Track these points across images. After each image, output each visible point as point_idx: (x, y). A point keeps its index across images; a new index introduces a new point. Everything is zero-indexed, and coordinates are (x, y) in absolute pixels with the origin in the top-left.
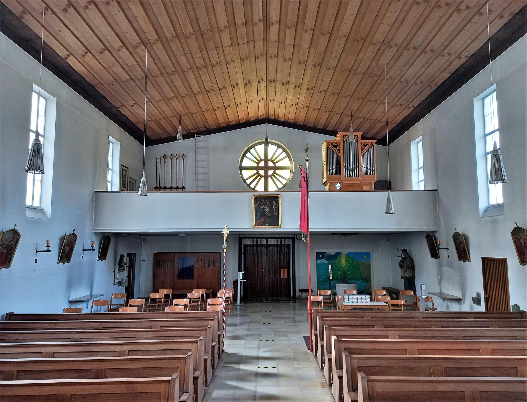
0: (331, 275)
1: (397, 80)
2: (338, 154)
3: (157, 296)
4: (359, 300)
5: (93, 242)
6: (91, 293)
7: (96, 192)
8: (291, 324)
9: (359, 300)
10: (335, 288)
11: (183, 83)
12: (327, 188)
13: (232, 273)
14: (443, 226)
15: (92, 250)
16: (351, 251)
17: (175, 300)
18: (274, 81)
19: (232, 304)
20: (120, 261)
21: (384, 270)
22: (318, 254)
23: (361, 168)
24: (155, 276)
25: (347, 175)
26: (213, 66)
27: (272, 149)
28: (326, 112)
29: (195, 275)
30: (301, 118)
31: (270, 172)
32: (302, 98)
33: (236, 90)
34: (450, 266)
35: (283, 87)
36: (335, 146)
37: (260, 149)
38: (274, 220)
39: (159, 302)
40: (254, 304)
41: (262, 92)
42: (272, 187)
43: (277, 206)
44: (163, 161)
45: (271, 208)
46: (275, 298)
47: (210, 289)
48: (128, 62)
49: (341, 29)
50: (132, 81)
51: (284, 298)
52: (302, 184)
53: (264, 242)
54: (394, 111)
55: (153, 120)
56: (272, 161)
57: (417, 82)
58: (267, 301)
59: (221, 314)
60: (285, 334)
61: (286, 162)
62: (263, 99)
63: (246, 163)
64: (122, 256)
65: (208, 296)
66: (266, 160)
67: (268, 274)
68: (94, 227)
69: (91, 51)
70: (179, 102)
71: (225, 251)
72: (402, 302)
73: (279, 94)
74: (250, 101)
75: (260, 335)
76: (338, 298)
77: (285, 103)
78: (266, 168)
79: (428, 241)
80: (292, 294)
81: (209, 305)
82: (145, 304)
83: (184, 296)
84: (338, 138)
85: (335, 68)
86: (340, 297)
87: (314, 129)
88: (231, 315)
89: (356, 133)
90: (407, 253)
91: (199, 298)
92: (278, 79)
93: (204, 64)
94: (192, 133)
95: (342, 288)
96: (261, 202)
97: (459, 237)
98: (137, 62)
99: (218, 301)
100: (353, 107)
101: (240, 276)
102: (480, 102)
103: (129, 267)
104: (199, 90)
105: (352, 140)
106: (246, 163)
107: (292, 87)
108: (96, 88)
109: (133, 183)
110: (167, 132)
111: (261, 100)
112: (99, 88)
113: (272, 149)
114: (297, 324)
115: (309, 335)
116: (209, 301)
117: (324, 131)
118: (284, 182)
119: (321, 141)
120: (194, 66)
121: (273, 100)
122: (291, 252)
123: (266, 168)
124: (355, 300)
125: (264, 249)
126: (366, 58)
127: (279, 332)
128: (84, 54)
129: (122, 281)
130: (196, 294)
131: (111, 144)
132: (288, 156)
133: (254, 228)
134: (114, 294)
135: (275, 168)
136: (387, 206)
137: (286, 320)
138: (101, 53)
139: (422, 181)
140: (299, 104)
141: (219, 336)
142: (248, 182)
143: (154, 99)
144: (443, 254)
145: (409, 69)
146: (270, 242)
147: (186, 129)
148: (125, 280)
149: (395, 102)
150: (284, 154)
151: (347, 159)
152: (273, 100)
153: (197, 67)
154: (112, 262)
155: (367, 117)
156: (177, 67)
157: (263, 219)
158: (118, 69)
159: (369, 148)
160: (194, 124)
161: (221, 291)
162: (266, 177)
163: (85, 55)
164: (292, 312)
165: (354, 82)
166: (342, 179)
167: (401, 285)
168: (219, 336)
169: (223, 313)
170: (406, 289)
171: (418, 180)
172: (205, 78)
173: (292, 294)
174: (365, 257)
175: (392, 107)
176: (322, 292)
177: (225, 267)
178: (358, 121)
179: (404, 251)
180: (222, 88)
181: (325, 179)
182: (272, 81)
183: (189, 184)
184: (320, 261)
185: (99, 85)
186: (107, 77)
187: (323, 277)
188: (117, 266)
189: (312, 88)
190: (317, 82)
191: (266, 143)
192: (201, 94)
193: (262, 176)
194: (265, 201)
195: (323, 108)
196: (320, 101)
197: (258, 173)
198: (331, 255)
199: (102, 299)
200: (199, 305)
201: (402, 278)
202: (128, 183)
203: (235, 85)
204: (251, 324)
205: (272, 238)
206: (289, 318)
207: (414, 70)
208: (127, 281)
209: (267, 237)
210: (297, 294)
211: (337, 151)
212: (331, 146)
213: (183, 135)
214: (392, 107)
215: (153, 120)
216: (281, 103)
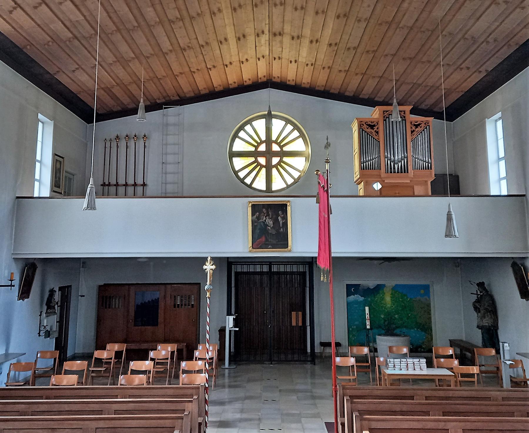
1: (460, 36)
2: (376, 137)
3: (104, 355)
4: (411, 366)
5: (12, 274)
6: (7, 350)
7: (18, 198)
8: (306, 402)
9: (411, 366)
10: (375, 341)
11: (148, 40)
12: (361, 189)
13: (217, 317)
15: (11, 286)
16: (399, 283)
17: (132, 363)
18: (280, 34)
19: (216, 368)
20: (48, 299)
21: (451, 316)
23: (410, 159)
24: (99, 320)
25: (391, 171)
26: (192, 18)
27: (277, 125)
28: (357, 74)
29: (161, 319)
30: (321, 80)
31: (275, 160)
32: (321, 56)
33: (224, 47)
35: (294, 42)
36: (372, 127)
37: (260, 125)
38: (282, 240)
39: (107, 363)
40: (252, 366)
41: (263, 48)
42: (278, 184)
43: (285, 218)
44: (114, 144)
45: (276, 221)
46: (283, 357)
47: (183, 342)
48: (71, 17)
50: (76, 41)
51: (296, 357)
52: (320, 188)
53: (265, 269)
54: (457, 77)
55: (102, 89)
56: (278, 147)
57: (489, 39)
58: (271, 361)
59: (202, 390)
60: (297, 418)
61: (299, 145)
62: (263, 57)
63: (239, 146)
64: (52, 292)
65: (181, 358)
66: (269, 141)
67: (271, 314)
68: (14, 250)
69: (22, 6)
70: (141, 63)
71: (208, 295)
72: (475, 370)
73: (288, 50)
74: (244, 60)
75: (259, 419)
76: (379, 361)
77: (296, 61)
78: (269, 154)
80: (309, 350)
81: (184, 372)
82: (88, 369)
83: (143, 356)
85: (368, 20)
86: (382, 359)
87: (340, 96)
88: (215, 386)
89: (402, 108)
90: (485, 289)
91: (167, 359)
92: (285, 31)
93: (179, 17)
94: (159, 104)
95: (385, 343)
96: (261, 212)
98: (85, 16)
99: (197, 364)
100: (397, 69)
101: (230, 321)
103: (62, 307)
104: (171, 48)
105: (396, 117)
106: (239, 146)
107: (306, 42)
108: (24, 50)
109: (70, 179)
110: (123, 104)
111: (261, 58)
112: (28, 51)
113: (277, 125)
114: (317, 401)
115: (333, 421)
116: (183, 364)
117: (355, 99)
118: (296, 175)
119: (353, 114)
120: (166, 19)
121: (279, 58)
122: (308, 285)
123: (269, 154)
124: (403, 365)
125: (265, 278)
127: (288, 415)
128: (11, 9)
129: (51, 329)
130: (164, 351)
131: (40, 125)
132: (302, 135)
133: (250, 251)
134: (41, 352)
135: (283, 154)
136: (447, 226)
137: (300, 394)
138: (35, 8)
139: (504, 178)
140: (317, 63)
141: (200, 424)
142: (242, 175)
143: (104, 61)
145: (475, 23)
146: (275, 269)
147: (150, 97)
148: (55, 328)
149: (459, 63)
150: (296, 134)
151: (389, 145)
152: (279, 58)
153: (169, 20)
154: (37, 301)
155: (420, 82)
156: (141, 20)
157: (263, 239)
158: (58, 26)
159: (422, 128)
160: (162, 91)
161: (200, 347)
162: (269, 167)
163: (12, 11)
164: (309, 380)
165: (397, 39)
166: (382, 176)
167: (477, 338)
168: (200, 424)
169: (206, 389)
170: (485, 346)
171: (498, 180)
172: (180, 33)
173: (309, 350)
174: (422, 292)
175: (456, 70)
176: (355, 350)
177: (208, 320)
178: (405, 88)
179: (481, 285)
180: (204, 44)
181: (357, 175)
182: (277, 33)
183: (153, 180)
184: (352, 298)
185: (28, 47)
186: (41, 36)
187: (357, 323)
188: (45, 307)
189: (336, 44)
190: (343, 37)
191: (269, 117)
192: (174, 53)
193: (262, 166)
194: (267, 210)
195: (353, 69)
196: (348, 61)
197: (256, 161)
198: (369, 288)
199: (24, 360)
200: (167, 372)
201: (478, 327)
202: (65, 184)
203: (223, 40)
204: (246, 401)
206: (306, 391)
207: (482, 24)
208: (58, 330)
209: (270, 262)
210: (318, 349)
211: (374, 133)
213: (145, 106)
214: (456, 70)
215: (102, 89)
216: (291, 62)
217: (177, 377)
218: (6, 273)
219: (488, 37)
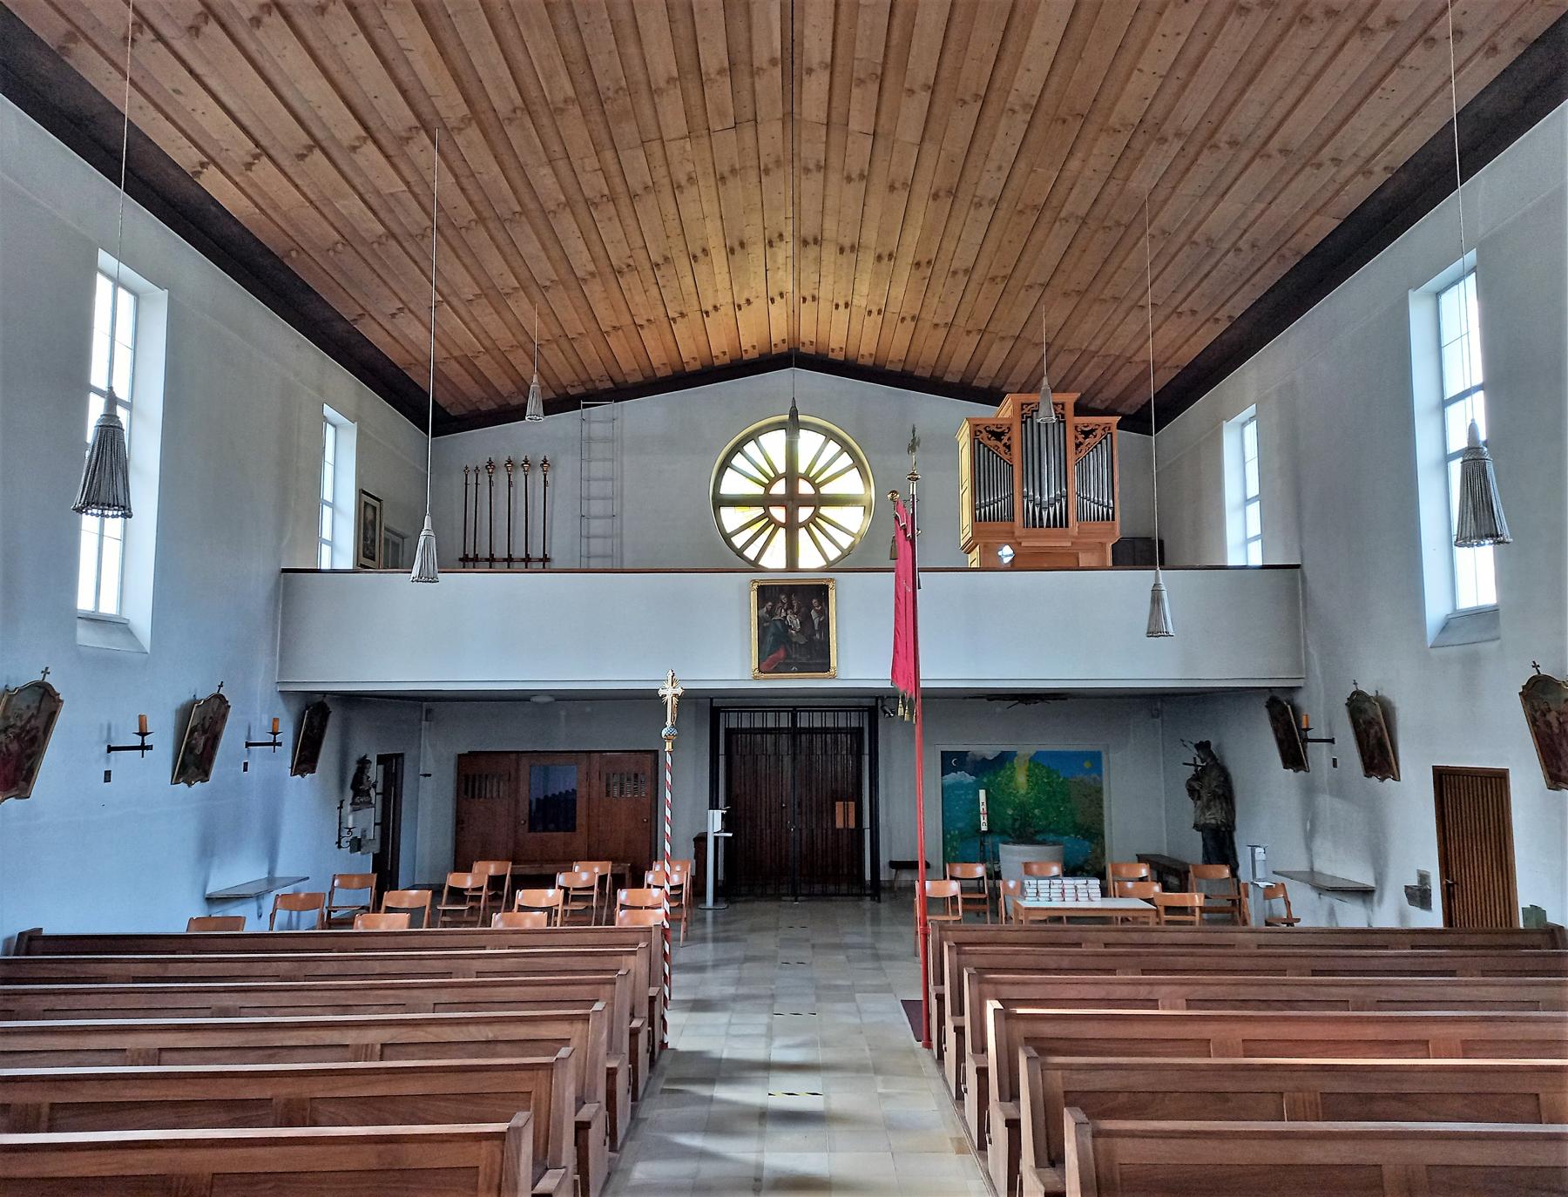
0: (984, 820)
1: (1182, 237)
2: (1006, 457)
3: (467, 881)
4: (1069, 892)
5: (276, 720)
6: (271, 871)
7: (285, 571)
8: (864, 965)
9: (1069, 892)
10: (996, 858)
11: (544, 248)
13: (691, 814)
14: (1318, 673)
15: (274, 744)
16: (1043, 749)
17: (520, 894)
18: (816, 241)
19: (689, 905)
20: (356, 776)
21: (1143, 803)
22: (945, 756)
23: (1073, 500)
24: (460, 823)
25: (1034, 522)
26: (633, 197)
27: (809, 442)
28: (969, 332)
29: (581, 819)
30: (896, 352)
31: (804, 513)
32: (898, 292)
33: (701, 269)
34: (1339, 791)
35: (843, 259)
36: (998, 436)
37: (775, 443)
38: (817, 655)
39: (473, 898)
40: (756, 905)
42: (809, 558)
43: (824, 613)
44: (484, 478)
45: (806, 620)
46: (818, 888)
47: (624, 860)
48: (379, 183)
49: (1016, 86)
50: (393, 243)
51: (844, 888)
52: (899, 547)
53: (785, 722)
54: (1171, 332)
55: (456, 359)
56: (809, 481)
57: (1241, 244)
58: (795, 895)
59: (656, 936)
60: (847, 994)
61: (851, 484)
62: (781, 295)
63: (733, 484)
64: (363, 763)
65: (619, 882)
66: (791, 476)
67: (798, 817)
68: (280, 676)
69: (272, 152)
70: (532, 302)
71: (669, 746)
72: (1197, 900)
73: (831, 279)
74: (743, 302)
75: (773, 996)
76: (1006, 887)
77: (847, 305)
78: (792, 501)
79: (1274, 719)
80: (868, 877)
81: (623, 907)
82: (433, 906)
83: (548, 882)
84: (1006, 411)
85: (997, 204)
86: (1012, 884)
87: (934, 385)
88: (686, 939)
89: (1060, 397)
90: (1211, 754)
91: (592, 888)
92: (826, 235)
93: (606, 192)
94: (573, 397)
95: (1016, 858)
96: (776, 601)
97: (1367, 705)
98: (407, 183)
99: (650, 895)
100: (1051, 318)
101: (715, 821)
102: (1428, 304)
103: (385, 794)
104: (591, 267)
105: (1046, 415)
106: (733, 484)
107: (868, 259)
108: (286, 261)
109: (396, 545)
110: (498, 393)
111: (778, 299)
112: (295, 263)
113: (809, 442)
114: (884, 964)
115: (920, 997)
116: (623, 895)
117: (964, 390)
118: (846, 541)
119: (955, 421)
120: (579, 197)
121: (814, 298)
122: (867, 751)
123: (792, 501)
124: (1056, 892)
125: (784, 741)
126: (1088, 173)
127: (829, 987)
128: (250, 160)
129: (364, 836)
130: (584, 874)
131: (330, 430)
132: (858, 464)
133: (755, 678)
134: (340, 876)
135: (818, 501)
136: (1152, 614)
137: (851, 952)
138: (301, 157)
139: (1255, 538)
140: (891, 309)
141: (652, 1000)
142: (738, 541)
143: (457, 296)
144: (1318, 755)
145: (1216, 204)
146: (803, 722)
147: (554, 383)
148: (373, 833)
149: (1175, 303)
150: (846, 460)
151: (1032, 474)
152: (814, 298)
153: (586, 201)
154: (333, 781)
155: (1093, 348)
156: (527, 199)
157: (781, 653)
158: (351, 206)
159: (1097, 439)
160: (579, 368)
161: (657, 867)
162: (791, 527)
163: (252, 164)
164: (869, 928)
165: (1054, 244)
166: (1017, 533)
167: (1192, 848)
168: (652, 1000)
169: (665, 932)
170: (1208, 860)
171: (1244, 536)
172: (611, 232)
173: (868, 877)
174: (1087, 765)
175: (1167, 318)
176: (959, 870)
177: (668, 796)
178: (1064, 361)
179: (1203, 747)
180: (660, 261)
181: (966, 533)
182: (810, 240)
183: (561, 547)
184: (952, 777)
185: (294, 254)
186: (319, 231)
187: (960, 825)
188: (350, 794)
189: (929, 262)
190: (945, 243)
191: (793, 426)
192: (598, 280)
193: (778, 525)
194: (789, 597)
195: (961, 321)
196: (953, 301)
197: (767, 515)
198: (984, 759)
199: (305, 889)
200: (592, 909)
201: (1196, 826)
202: (380, 546)
203: (699, 254)
204: (748, 965)
205: (811, 709)
206: (861, 946)
207: (1230, 207)
208: (378, 838)
209: (794, 705)
210: (885, 875)
211: (1002, 449)
212: (985, 434)
213: (544, 402)
214: (1167, 318)
215: (456, 359)
216: (837, 306)
217: (611, 920)
218: (266, 722)
219: (1241, 237)
